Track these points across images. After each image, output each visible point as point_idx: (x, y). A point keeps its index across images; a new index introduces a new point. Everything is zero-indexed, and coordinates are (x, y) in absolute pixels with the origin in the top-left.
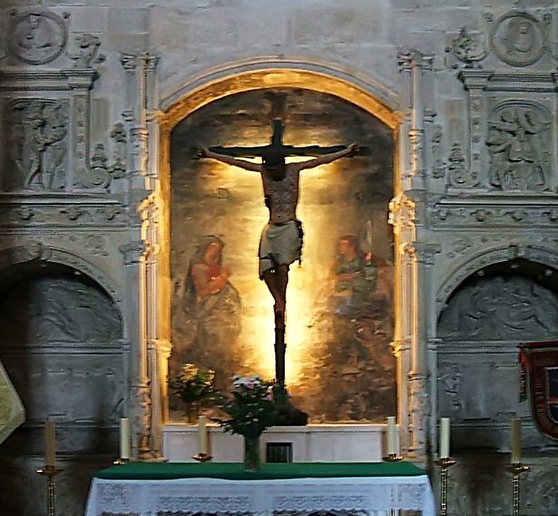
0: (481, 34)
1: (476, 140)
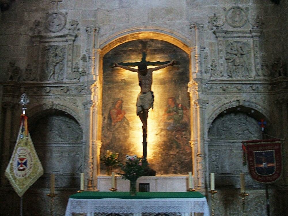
0: (222, 15)
1: (221, 58)
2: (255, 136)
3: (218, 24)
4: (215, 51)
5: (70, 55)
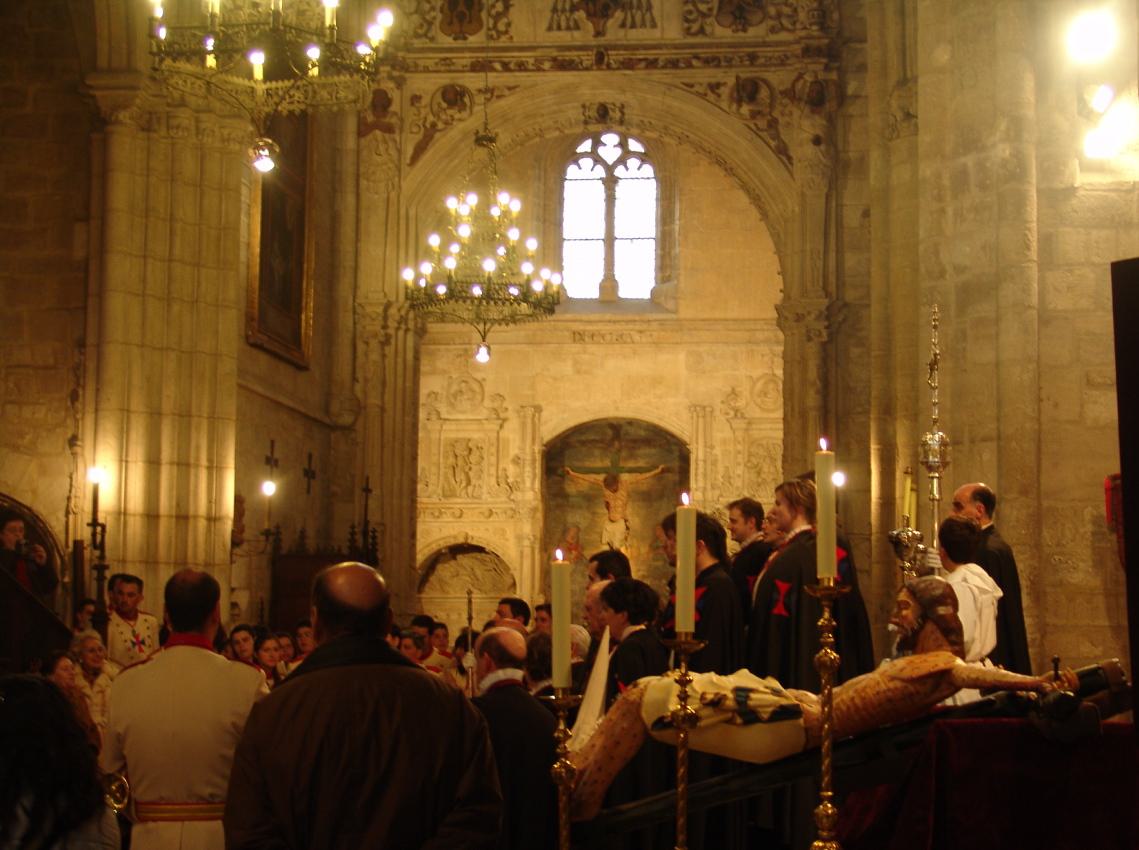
0: (744, 389)
1: (739, 464)
2: (666, 720)
3: (738, 404)
4: (730, 452)
5: (492, 455)
